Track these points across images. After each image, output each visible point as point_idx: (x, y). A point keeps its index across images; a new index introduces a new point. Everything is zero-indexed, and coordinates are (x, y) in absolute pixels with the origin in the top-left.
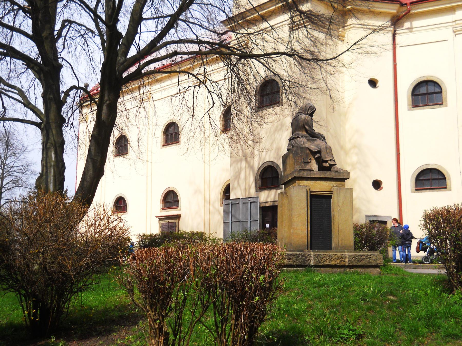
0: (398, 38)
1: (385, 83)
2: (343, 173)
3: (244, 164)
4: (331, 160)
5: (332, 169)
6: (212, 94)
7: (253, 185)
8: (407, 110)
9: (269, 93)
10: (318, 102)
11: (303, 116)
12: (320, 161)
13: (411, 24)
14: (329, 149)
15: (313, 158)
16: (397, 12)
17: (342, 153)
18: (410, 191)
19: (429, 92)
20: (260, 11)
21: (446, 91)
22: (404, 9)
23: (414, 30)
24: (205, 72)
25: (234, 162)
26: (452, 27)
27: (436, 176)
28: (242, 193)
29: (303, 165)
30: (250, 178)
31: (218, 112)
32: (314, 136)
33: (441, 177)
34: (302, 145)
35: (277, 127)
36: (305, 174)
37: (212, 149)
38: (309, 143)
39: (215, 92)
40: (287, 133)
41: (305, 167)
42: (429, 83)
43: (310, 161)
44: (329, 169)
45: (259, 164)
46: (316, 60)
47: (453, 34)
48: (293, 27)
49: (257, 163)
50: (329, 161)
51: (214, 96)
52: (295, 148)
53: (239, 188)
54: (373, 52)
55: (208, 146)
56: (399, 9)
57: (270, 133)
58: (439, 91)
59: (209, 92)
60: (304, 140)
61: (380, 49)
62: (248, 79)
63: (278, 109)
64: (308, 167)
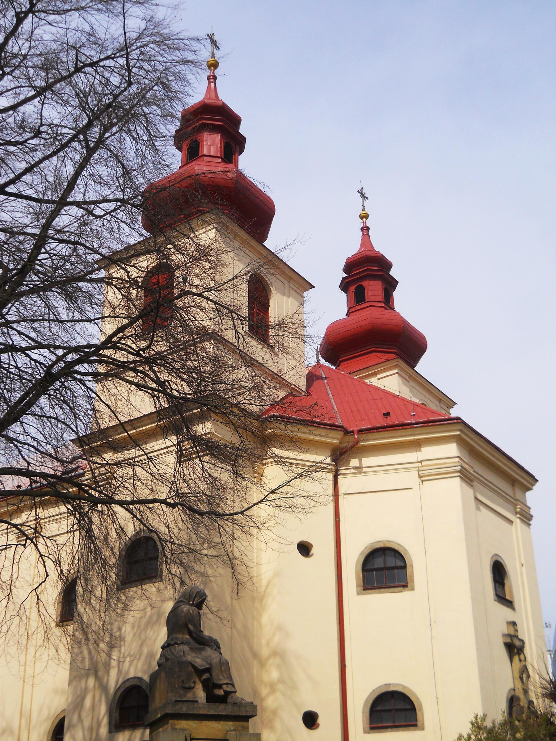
0: (342, 481)
1: (323, 549)
2: (245, 706)
3: (91, 682)
4: (227, 684)
5: (229, 700)
6: (46, 559)
7: (105, 721)
8: (355, 593)
9: (141, 560)
10: (216, 582)
11: (185, 608)
12: (210, 687)
13: (360, 462)
14: (225, 666)
15: (198, 681)
16: (340, 443)
17: (256, 663)
18: (362, 730)
19: (388, 565)
20: (130, 431)
21: (412, 566)
22: (350, 439)
23: (364, 470)
24: (37, 518)
25: (75, 677)
26: (417, 469)
27: (401, 705)
28: (84, 735)
29: (182, 692)
30: (100, 707)
31: (52, 592)
32: (203, 642)
33: (408, 707)
34: (181, 657)
35: (151, 617)
36: (184, 709)
37: (38, 654)
38: (194, 655)
39: (51, 556)
40: (161, 635)
41: (186, 696)
42: (387, 552)
43: (192, 685)
44: (223, 699)
45: (117, 681)
46: (213, 514)
47: (418, 480)
48: (181, 457)
49: (113, 680)
50: (225, 687)
51: (49, 563)
52: (169, 663)
53: (80, 726)
54: (299, 506)
55: (31, 650)
56: (342, 438)
57: (139, 626)
58: (402, 564)
59: (41, 556)
60: (186, 648)
61: (310, 501)
62: (106, 539)
63: (151, 588)
64: (189, 696)
